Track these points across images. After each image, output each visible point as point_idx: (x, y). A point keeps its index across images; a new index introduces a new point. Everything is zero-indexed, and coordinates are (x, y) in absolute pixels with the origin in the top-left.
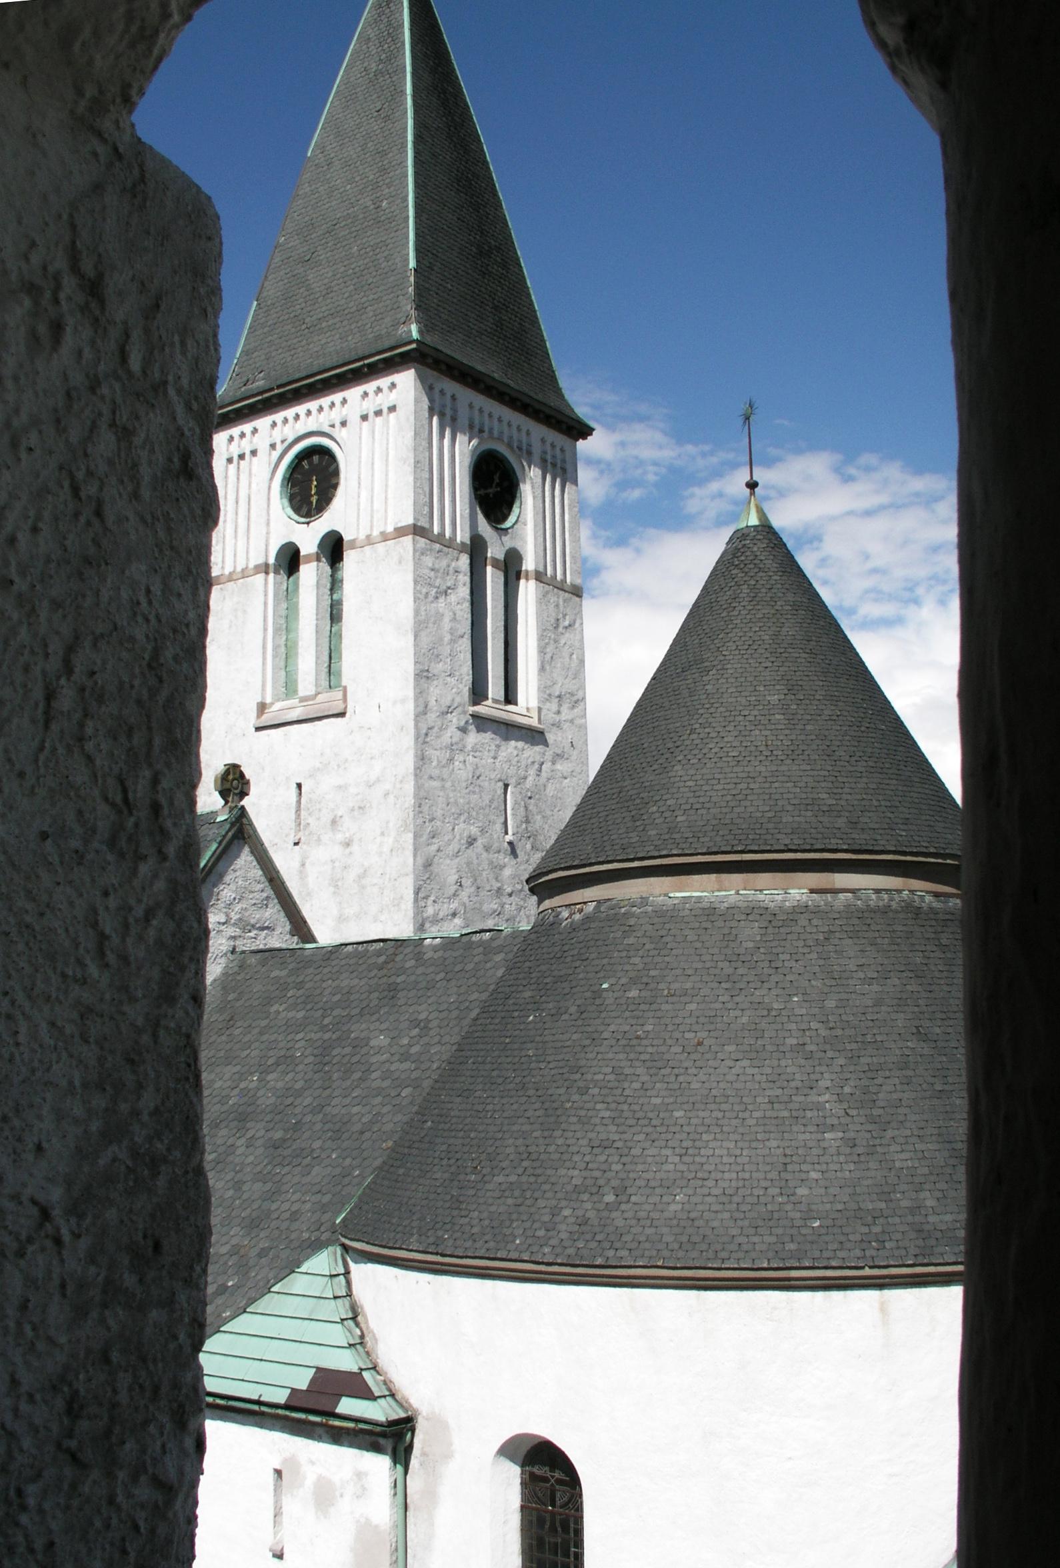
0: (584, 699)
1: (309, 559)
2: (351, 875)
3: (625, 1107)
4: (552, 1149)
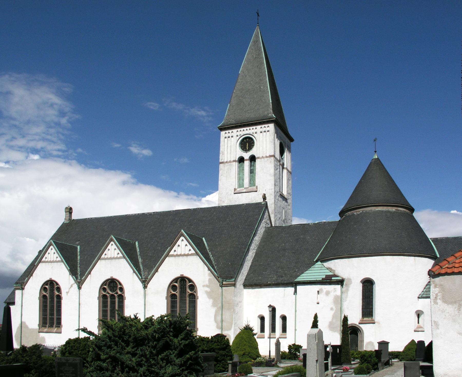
1: (247, 160)
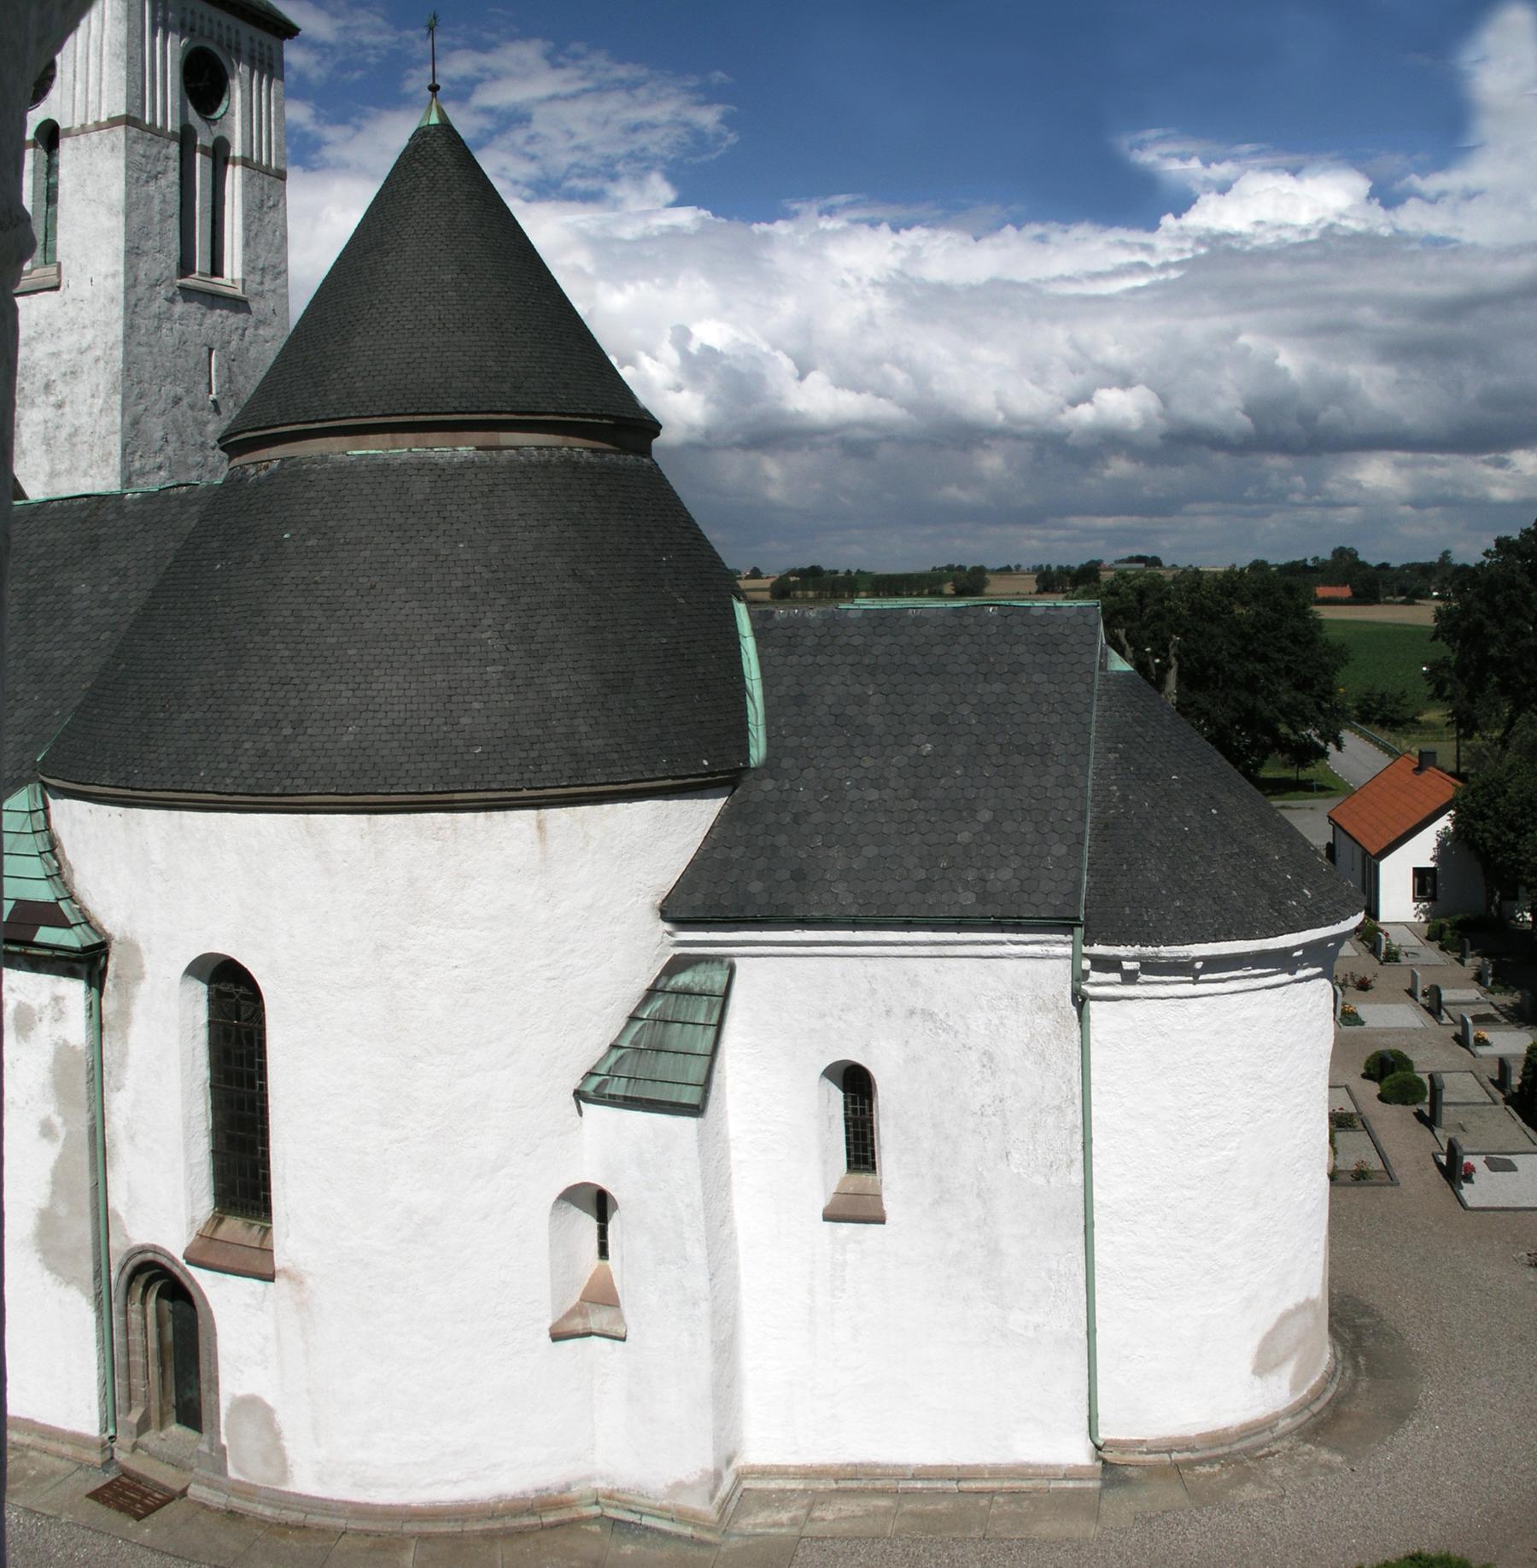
0: (286, 271)
2: (64, 433)
3: (303, 646)
4: (235, 686)
